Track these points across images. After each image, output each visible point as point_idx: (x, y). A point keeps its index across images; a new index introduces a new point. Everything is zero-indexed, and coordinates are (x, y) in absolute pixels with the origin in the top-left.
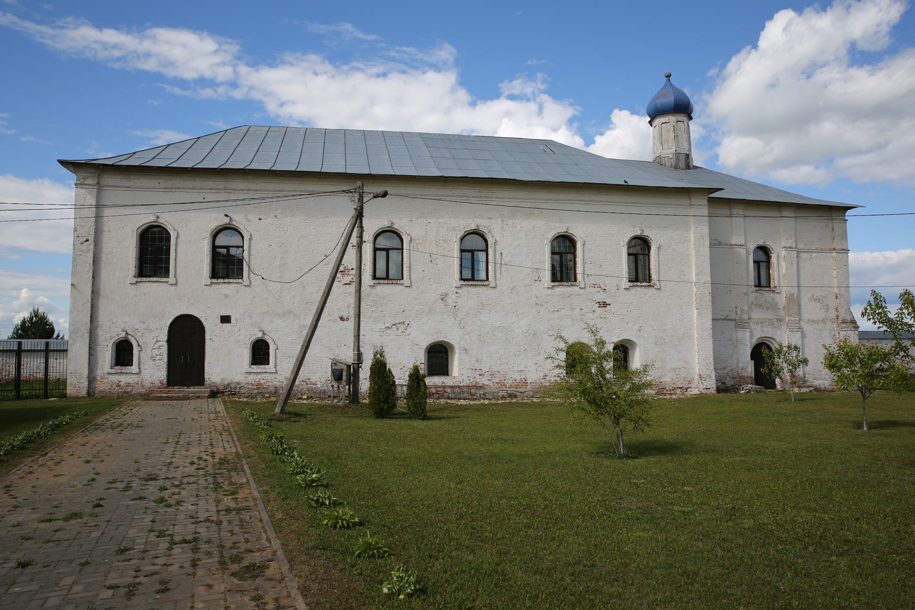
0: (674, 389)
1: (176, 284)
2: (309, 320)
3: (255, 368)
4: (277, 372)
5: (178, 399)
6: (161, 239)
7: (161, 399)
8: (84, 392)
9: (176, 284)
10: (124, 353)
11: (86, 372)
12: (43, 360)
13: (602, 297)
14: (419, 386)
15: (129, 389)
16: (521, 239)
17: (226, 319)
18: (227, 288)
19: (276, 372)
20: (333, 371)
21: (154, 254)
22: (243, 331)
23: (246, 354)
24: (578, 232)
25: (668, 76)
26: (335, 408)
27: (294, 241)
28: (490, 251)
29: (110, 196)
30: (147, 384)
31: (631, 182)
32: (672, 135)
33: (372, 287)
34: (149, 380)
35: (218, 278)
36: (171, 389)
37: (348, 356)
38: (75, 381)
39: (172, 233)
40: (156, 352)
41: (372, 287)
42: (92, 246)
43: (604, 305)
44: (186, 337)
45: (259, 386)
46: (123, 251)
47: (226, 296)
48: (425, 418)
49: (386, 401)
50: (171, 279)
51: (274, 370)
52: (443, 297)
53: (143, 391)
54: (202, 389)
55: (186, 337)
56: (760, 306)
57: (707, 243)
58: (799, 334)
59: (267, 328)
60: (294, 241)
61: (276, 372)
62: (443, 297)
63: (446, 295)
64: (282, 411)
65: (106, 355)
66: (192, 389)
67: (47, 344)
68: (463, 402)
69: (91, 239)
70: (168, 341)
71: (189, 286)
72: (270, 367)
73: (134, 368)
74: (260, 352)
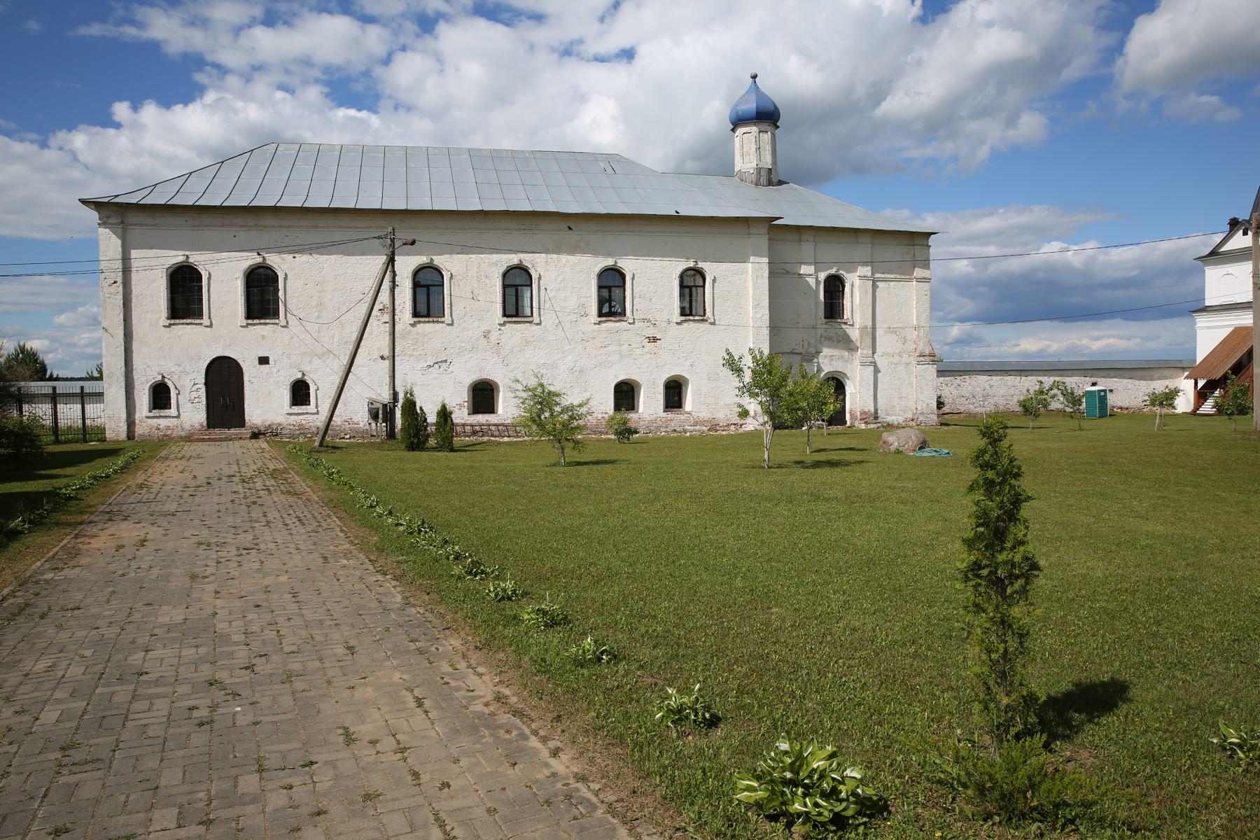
0: (728, 425)
1: (211, 326)
2: (345, 360)
3: (296, 409)
4: (313, 416)
5: (221, 440)
6: (192, 280)
7: (203, 440)
8: (123, 436)
9: (211, 326)
10: (161, 396)
11: (124, 416)
12: (79, 406)
13: (651, 332)
14: (446, 421)
15: (169, 432)
16: (566, 278)
17: (264, 361)
18: (263, 330)
19: (318, 413)
20: (370, 411)
21: (185, 295)
22: (282, 372)
23: (286, 395)
24: (627, 265)
25: (754, 77)
26: (371, 445)
27: (328, 285)
28: (535, 286)
29: (135, 233)
30: (187, 427)
31: (684, 212)
32: (754, 147)
33: (413, 325)
34: (189, 423)
35: (253, 318)
36: (211, 430)
37: (386, 397)
38: (114, 426)
39: (203, 273)
40: (194, 395)
41: (413, 325)
42: (121, 288)
43: (655, 340)
44: (224, 381)
45: (301, 427)
46: (152, 291)
47: (263, 337)
48: (452, 450)
49: (416, 435)
50: (205, 321)
51: (175, 414)
52: (486, 335)
53: (183, 434)
54: (243, 430)
55: (224, 381)
56: (830, 339)
57: (766, 274)
58: (872, 368)
59: (306, 368)
60: (328, 285)
61: (318, 413)
62: (486, 335)
63: (489, 332)
64: (321, 445)
65: (143, 399)
66: (232, 431)
67: (82, 388)
68: (506, 439)
69: (120, 280)
70: (206, 384)
71: (225, 327)
72: (311, 408)
73: (173, 411)
74: (300, 393)
